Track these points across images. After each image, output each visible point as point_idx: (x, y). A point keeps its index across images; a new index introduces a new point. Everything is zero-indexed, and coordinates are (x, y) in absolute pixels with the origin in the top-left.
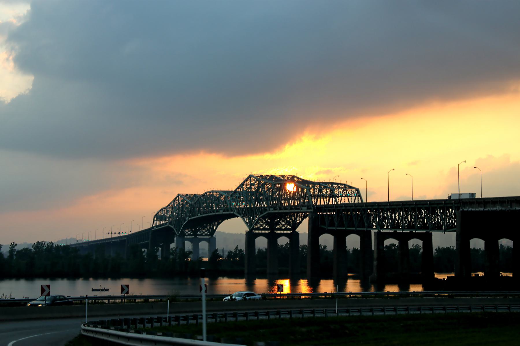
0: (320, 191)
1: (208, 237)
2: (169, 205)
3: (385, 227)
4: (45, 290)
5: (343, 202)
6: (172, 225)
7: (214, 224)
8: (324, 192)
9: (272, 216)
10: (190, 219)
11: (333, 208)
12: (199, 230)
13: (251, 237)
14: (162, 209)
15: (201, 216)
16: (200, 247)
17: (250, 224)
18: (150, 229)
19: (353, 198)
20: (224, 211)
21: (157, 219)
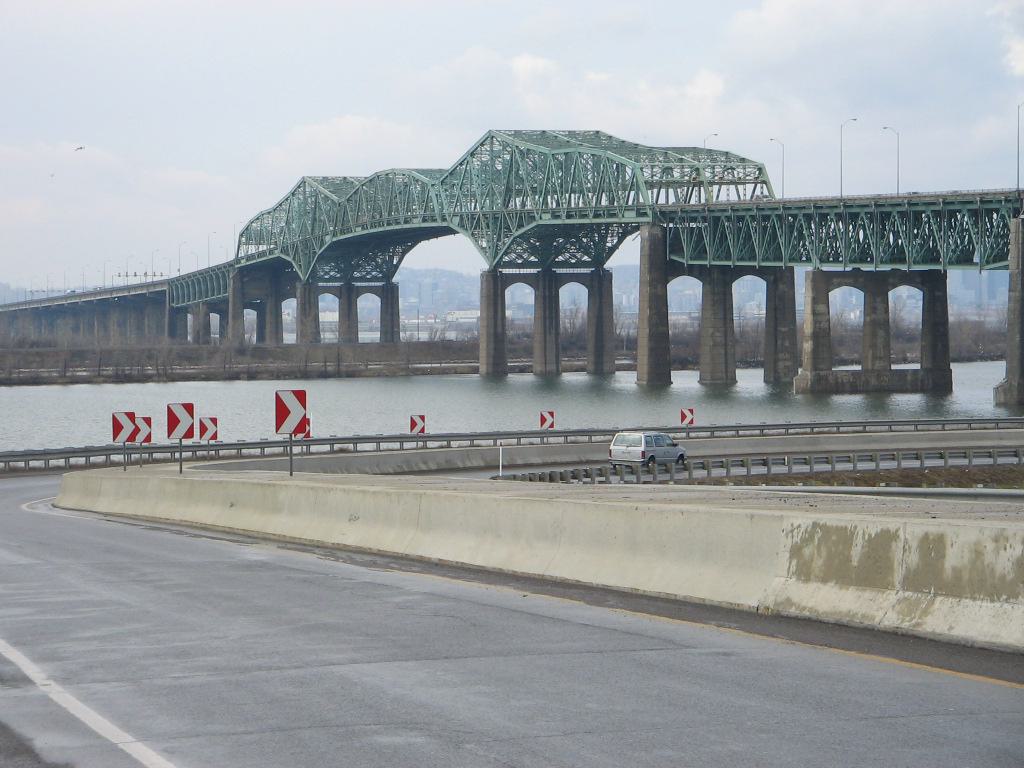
0: (668, 170)
1: (337, 284)
3: (804, 259)
5: (723, 198)
6: (288, 255)
7: (393, 252)
8: (676, 174)
9: (546, 234)
10: (335, 239)
11: (702, 214)
12: (358, 267)
13: (495, 284)
17: (493, 252)
18: (230, 265)
19: (750, 187)
20: (424, 220)
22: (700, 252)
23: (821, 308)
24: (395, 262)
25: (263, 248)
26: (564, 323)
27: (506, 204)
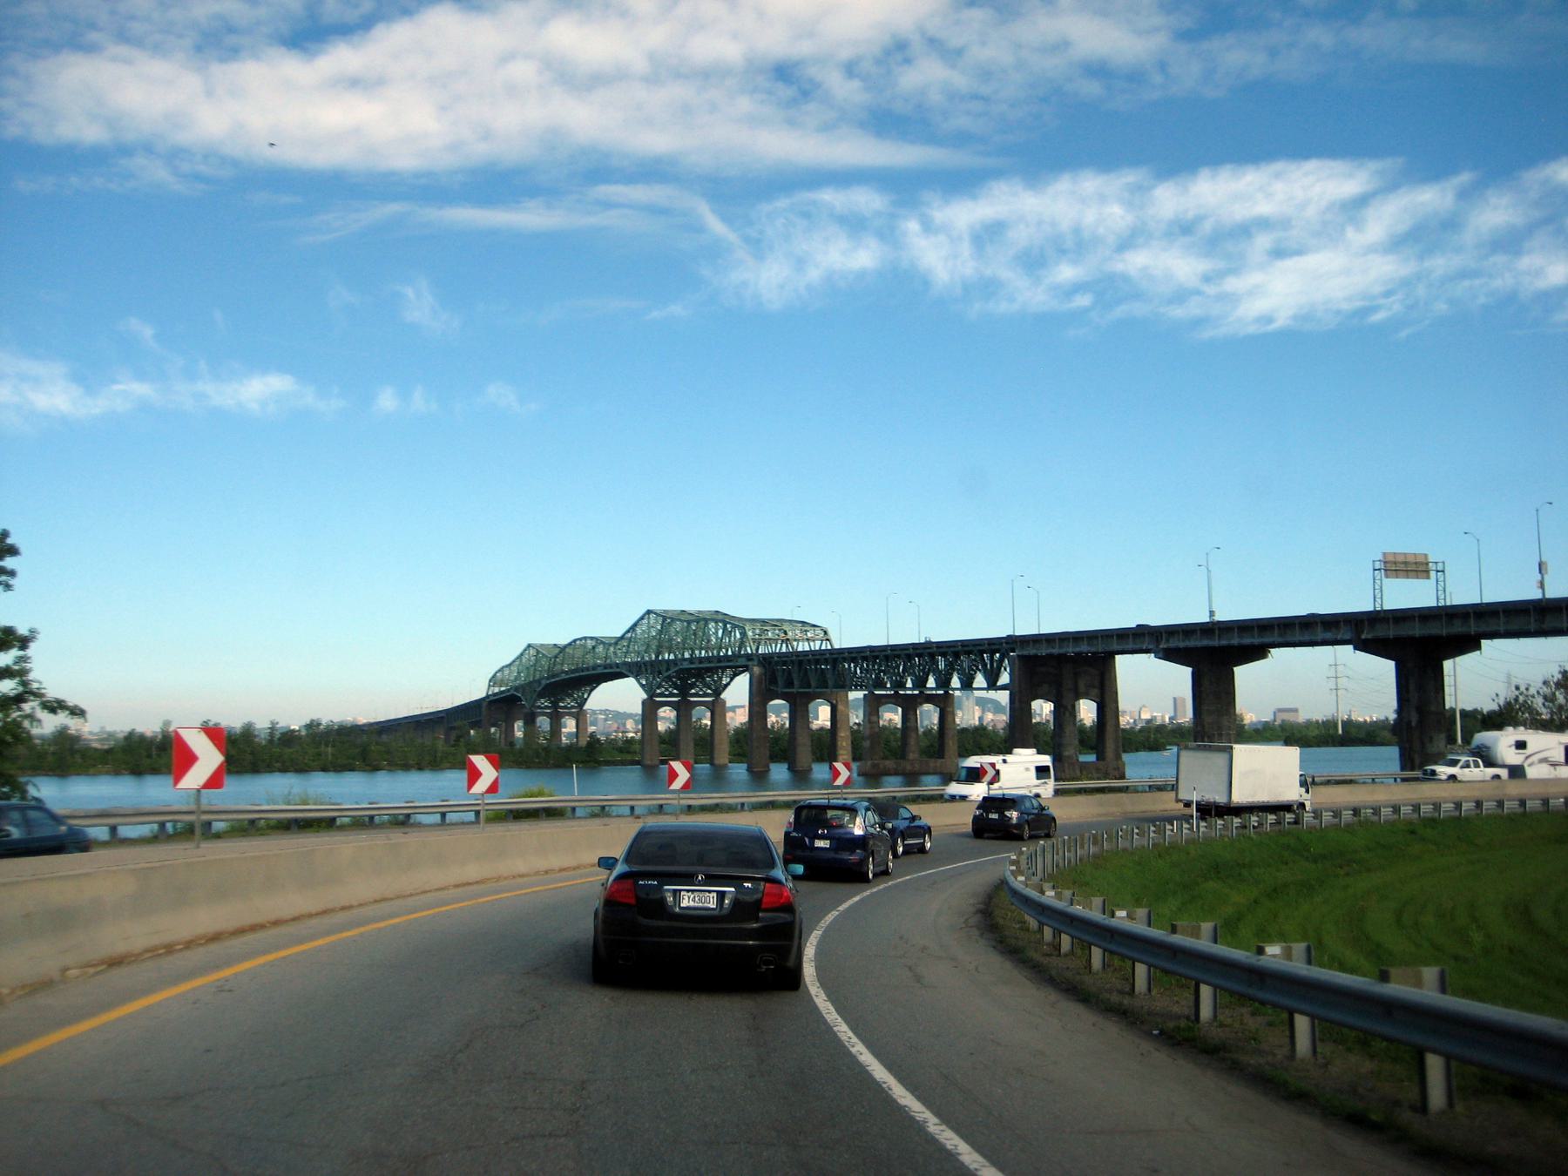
2: (514, 661)
4: (840, 774)
12: (562, 700)
14: (503, 667)
15: (568, 676)
16: (1033, 707)
18: (483, 699)
19: (818, 643)
21: (494, 683)
22: (790, 684)
23: (874, 718)
24: (585, 696)
25: (503, 689)
26: (1253, 292)
27: (657, 657)
